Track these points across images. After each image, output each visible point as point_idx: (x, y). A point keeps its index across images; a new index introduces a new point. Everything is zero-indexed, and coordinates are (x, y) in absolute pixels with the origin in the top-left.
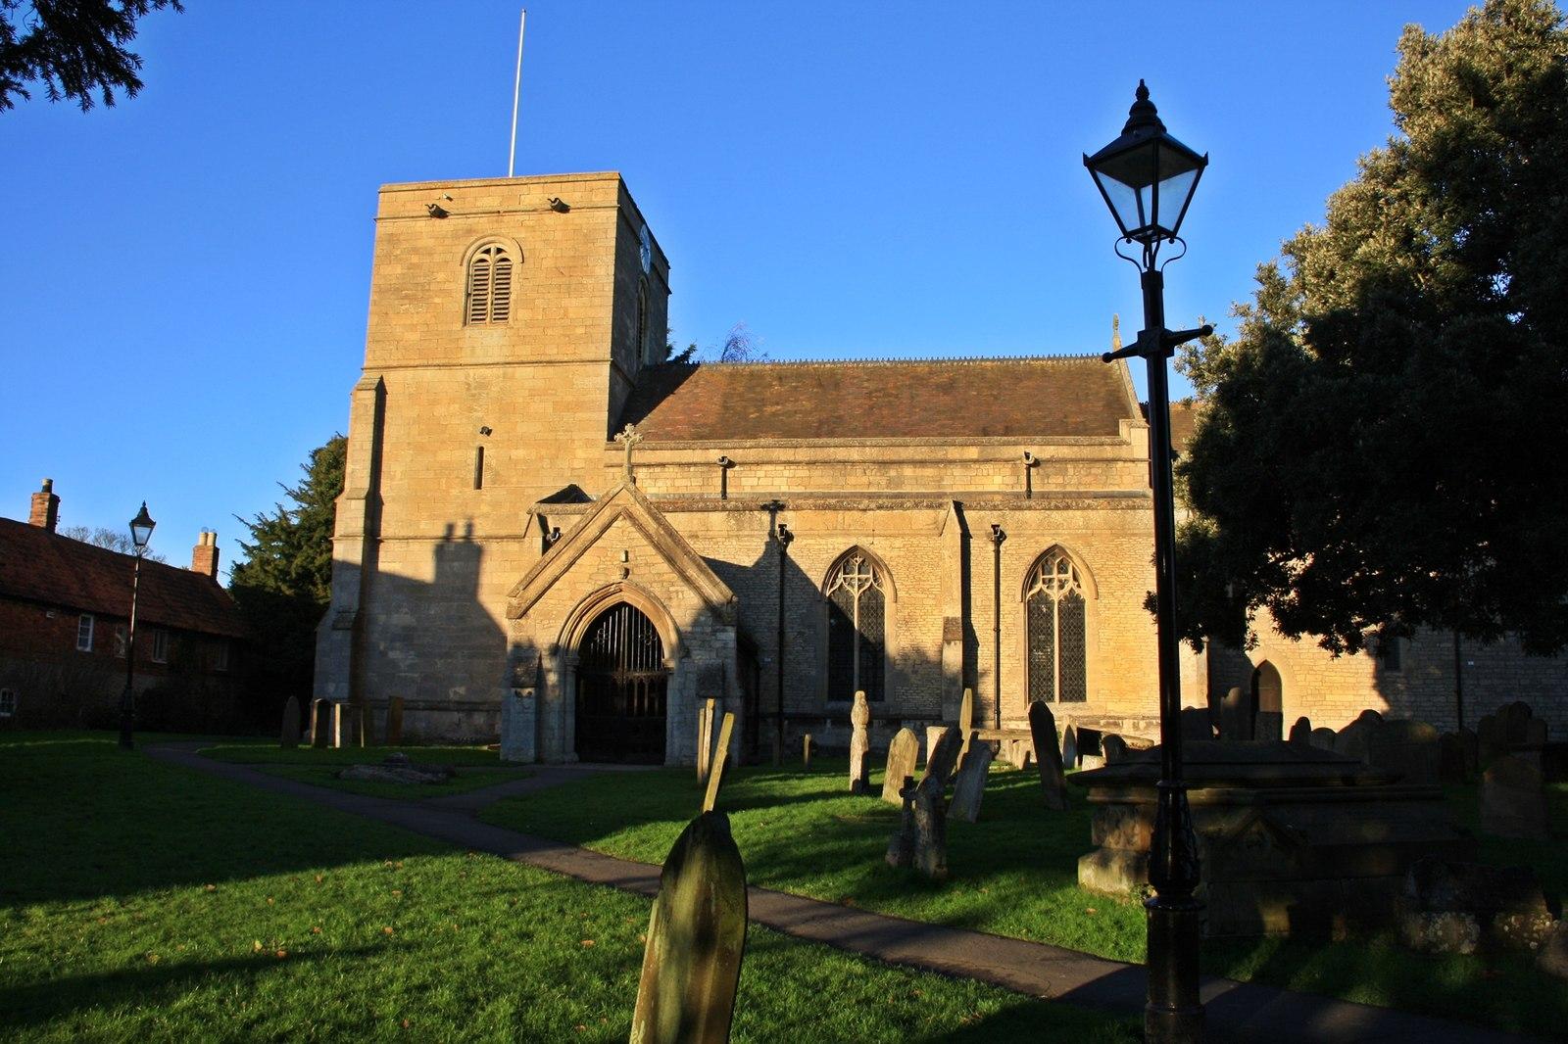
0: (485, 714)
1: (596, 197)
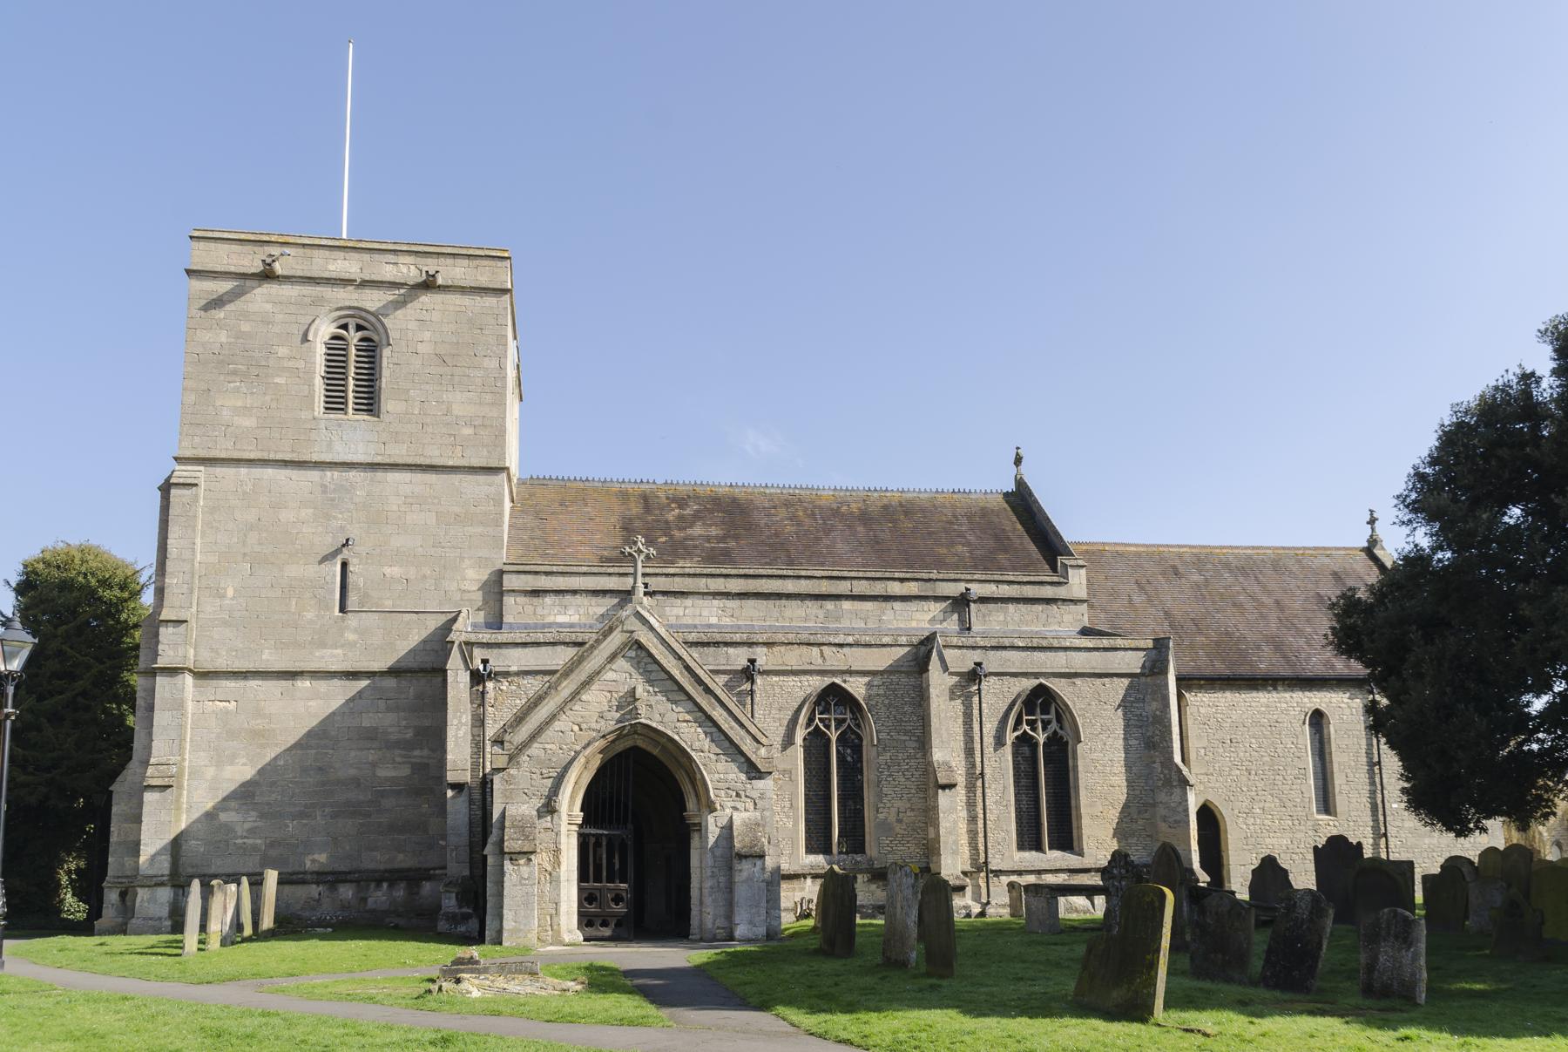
0: (354, 885)
1: (481, 275)
